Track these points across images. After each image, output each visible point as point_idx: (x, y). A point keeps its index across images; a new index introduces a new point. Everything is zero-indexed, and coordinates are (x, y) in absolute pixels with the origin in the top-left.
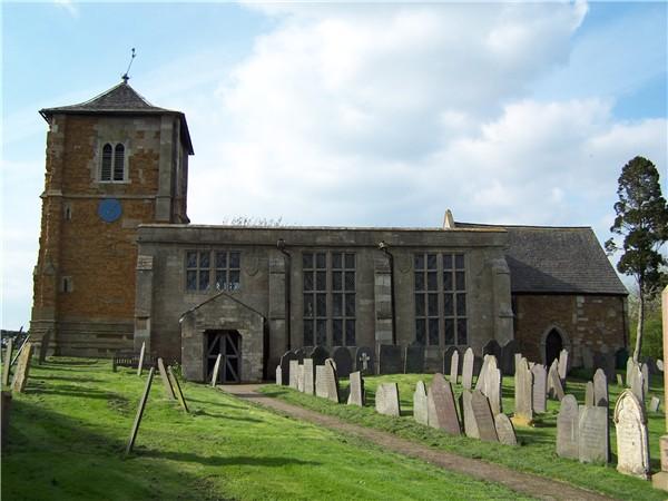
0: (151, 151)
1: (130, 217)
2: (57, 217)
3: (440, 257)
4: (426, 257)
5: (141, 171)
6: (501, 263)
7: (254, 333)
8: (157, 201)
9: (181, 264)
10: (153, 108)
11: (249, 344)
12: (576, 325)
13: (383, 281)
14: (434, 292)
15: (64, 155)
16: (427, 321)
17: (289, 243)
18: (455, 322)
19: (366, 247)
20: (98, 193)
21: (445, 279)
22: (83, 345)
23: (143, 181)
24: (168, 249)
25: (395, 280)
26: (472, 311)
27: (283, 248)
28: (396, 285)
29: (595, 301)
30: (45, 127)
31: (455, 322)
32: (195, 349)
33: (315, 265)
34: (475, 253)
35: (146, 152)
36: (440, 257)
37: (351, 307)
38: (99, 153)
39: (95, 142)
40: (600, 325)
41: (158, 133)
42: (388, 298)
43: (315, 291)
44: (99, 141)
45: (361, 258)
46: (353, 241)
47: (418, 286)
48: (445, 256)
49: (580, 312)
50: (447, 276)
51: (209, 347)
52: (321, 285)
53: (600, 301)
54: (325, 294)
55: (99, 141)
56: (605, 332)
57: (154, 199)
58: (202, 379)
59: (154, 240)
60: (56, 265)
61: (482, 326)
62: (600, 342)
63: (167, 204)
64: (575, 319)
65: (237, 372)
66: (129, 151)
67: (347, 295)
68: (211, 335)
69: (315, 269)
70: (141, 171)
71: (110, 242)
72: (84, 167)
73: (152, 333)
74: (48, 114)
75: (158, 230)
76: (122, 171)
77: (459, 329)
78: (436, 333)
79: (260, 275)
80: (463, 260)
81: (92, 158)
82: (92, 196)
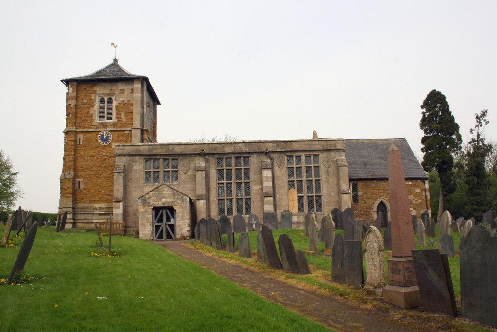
2: (73, 143)
5: (123, 114)
6: (342, 158)
8: (133, 131)
10: (129, 75)
11: (181, 215)
15: (76, 106)
17: (207, 152)
18: (315, 198)
19: (256, 152)
21: (307, 171)
22: (90, 221)
23: (124, 120)
24: (133, 158)
25: (275, 173)
26: (324, 191)
27: (202, 155)
28: (275, 176)
30: (65, 89)
31: (315, 198)
32: (147, 219)
34: (325, 154)
35: (125, 102)
36: (303, 158)
37: (300, 207)
38: (97, 103)
39: (95, 98)
41: (132, 90)
42: (270, 184)
43: (225, 181)
44: (97, 96)
45: (254, 160)
46: (248, 150)
51: (156, 218)
52: (229, 177)
53: (410, 183)
54: (231, 183)
56: (414, 202)
63: (139, 132)
65: (173, 233)
66: (116, 101)
67: (245, 183)
68: (157, 210)
69: (243, 167)
70: (123, 114)
71: (105, 157)
72: (88, 113)
74: (67, 82)
75: (127, 148)
76: (111, 114)
77: (317, 203)
78: (303, 206)
79: (190, 173)
82: (93, 130)
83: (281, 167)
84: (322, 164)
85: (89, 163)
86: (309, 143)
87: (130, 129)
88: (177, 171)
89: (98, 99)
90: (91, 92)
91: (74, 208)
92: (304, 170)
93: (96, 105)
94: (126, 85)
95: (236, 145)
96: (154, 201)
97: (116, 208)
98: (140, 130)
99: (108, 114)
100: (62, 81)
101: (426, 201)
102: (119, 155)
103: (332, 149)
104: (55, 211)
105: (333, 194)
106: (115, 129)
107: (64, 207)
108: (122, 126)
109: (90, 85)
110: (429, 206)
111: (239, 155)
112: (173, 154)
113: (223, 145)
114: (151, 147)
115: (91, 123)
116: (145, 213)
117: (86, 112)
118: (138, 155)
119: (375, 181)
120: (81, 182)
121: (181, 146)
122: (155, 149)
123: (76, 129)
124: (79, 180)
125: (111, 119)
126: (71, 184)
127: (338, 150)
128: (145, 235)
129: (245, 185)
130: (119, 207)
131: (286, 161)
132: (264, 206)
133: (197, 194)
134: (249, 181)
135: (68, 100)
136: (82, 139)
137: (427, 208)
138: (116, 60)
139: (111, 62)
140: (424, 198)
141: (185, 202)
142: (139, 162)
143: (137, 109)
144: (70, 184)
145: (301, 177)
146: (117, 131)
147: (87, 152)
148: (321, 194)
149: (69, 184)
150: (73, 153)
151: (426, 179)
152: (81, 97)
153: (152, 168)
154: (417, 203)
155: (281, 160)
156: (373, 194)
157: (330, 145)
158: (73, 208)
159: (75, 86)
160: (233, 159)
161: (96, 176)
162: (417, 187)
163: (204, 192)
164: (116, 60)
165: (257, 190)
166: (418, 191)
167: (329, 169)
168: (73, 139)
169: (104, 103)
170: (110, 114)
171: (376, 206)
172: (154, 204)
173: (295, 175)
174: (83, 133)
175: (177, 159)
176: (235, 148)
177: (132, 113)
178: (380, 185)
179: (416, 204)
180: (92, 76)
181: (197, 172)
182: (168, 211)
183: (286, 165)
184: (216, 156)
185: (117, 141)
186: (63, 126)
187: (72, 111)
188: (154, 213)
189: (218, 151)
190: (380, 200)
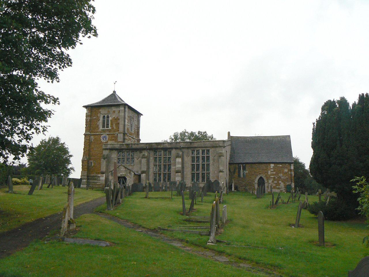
0: (117, 117)
3: (201, 151)
5: (114, 125)
9: (116, 156)
13: (179, 160)
15: (90, 121)
23: (115, 128)
29: (278, 166)
30: (85, 111)
39: (100, 116)
40: (281, 175)
41: (119, 111)
42: (180, 166)
45: (174, 152)
47: (193, 161)
49: (272, 170)
55: (101, 115)
56: (282, 178)
58: (181, 197)
62: (280, 182)
63: (122, 135)
64: (269, 173)
70: (114, 125)
73: (105, 178)
74: (86, 107)
80: (209, 152)
81: (99, 121)
85: (96, 152)
88: (134, 158)
89: (102, 116)
91: (88, 176)
92: (201, 158)
100: (84, 107)
101: (291, 177)
104: (79, 178)
105: (216, 172)
106: (110, 133)
108: (114, 132)
110: (293, 181)
119: (257, 164)
125: (108, 127)
129: (168, 166)
130: (103, 176)
131: (191, 153)
136: (93, 139)
137: (291, 182)
138: (114, 92)
140: (290, 175)
144: (86, 164)
148: (209, 172)
150: (88, 146)
151: (292, 163)
156: (255, 172)
157: (215, 144)
158: (87, 176)
162: (285, 168)
164: (114, 92)
167: (214, 158)
170: (108, 125)
171: (256, 181)
173: (195, 161)
179: (283, 179)
180: (100, 102)
182: (123, 179)
184: (154, 150)
185: (111, 140)
190: (260, 176)
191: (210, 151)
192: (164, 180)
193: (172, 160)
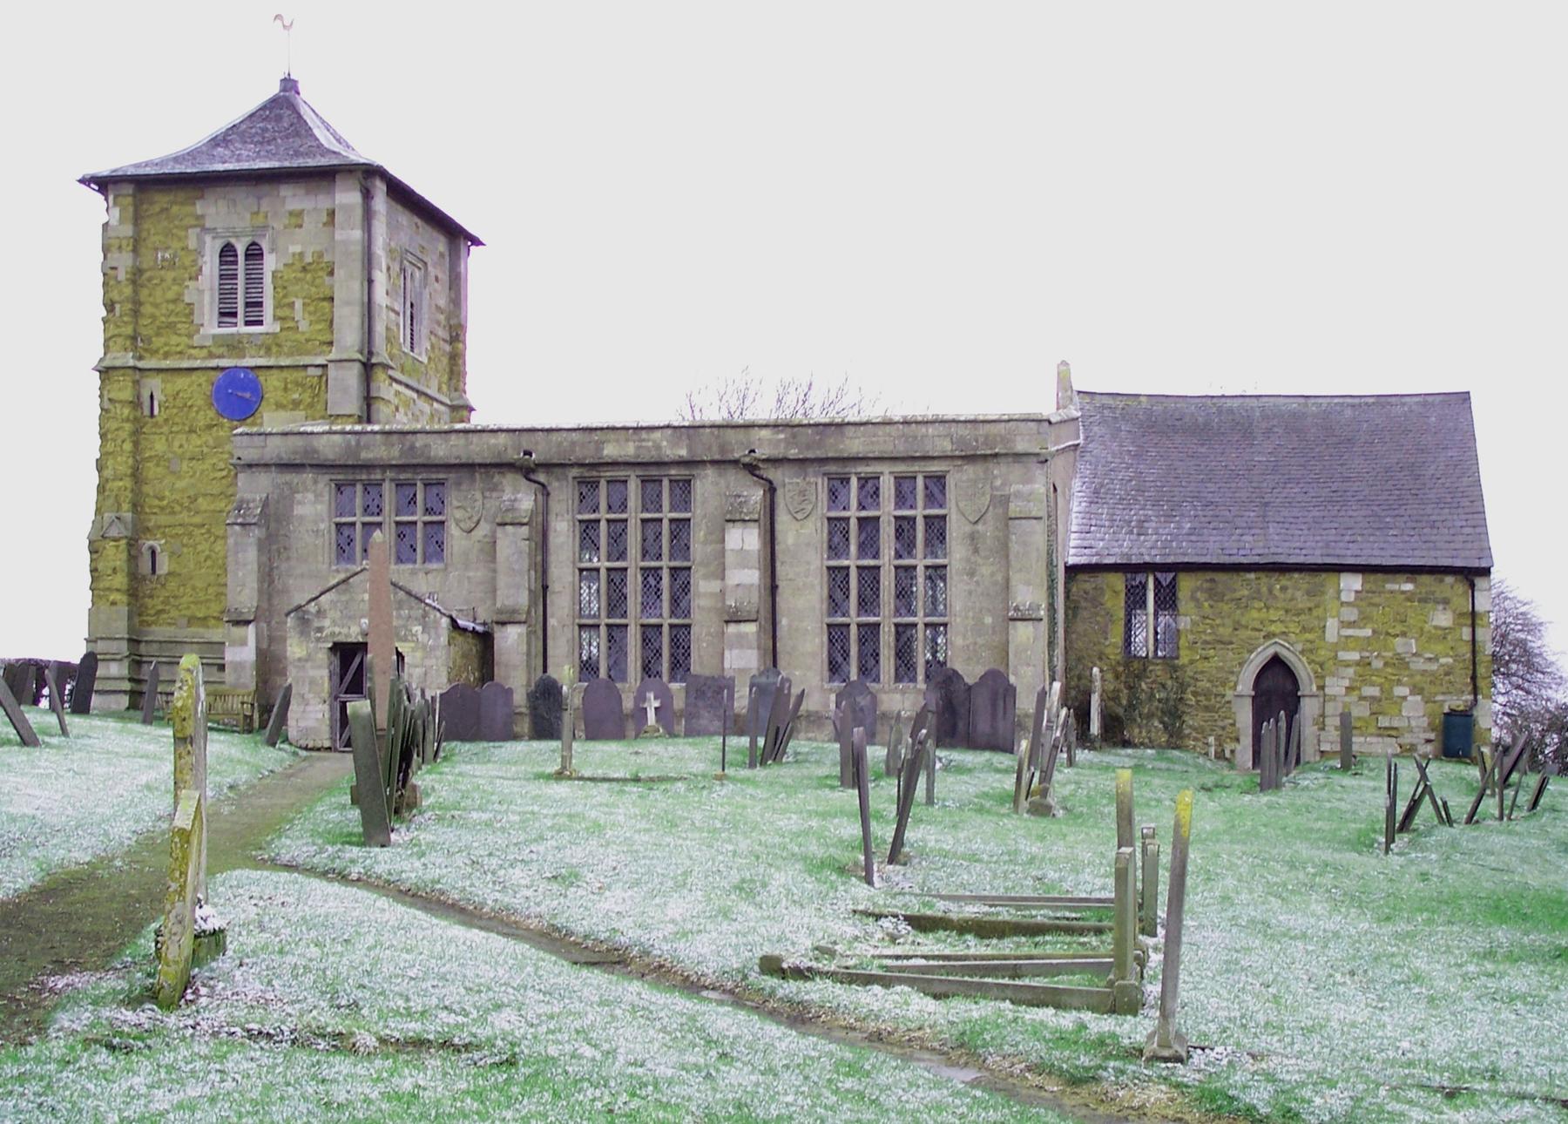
1: (280, 406)
3: (887, 486)
4: (854, 481)
5: (298, 304)
7: (428, 651)
9: (322, 508)
12: (1336, 647)
13: (745, 540)
14: (872, 562)
15: (137, 275)
16: (854, 630)
19: (714, 462)
20: (211, 356)
29: (1389, 586)
30: (95, 208)
32: (312, 682)
33: (603, 506)
34: (971, 471)
35: (309, 259)
36: (887, 486)
38: (210, 265)
39: (201, 242)
41: (332, 214)
44: (208, 238)
45: (708, 488)
47: (836, 547)
48: (899, 480)
49: (1351, 614)
50: (904, 528)
53: (1409, 587)
57: (324, 366)
58: (327, 744)
59: (267, 459)
60: (128, 516)
61: (980, 641)
63: (352, 375)
64: (1332, 633)
67: (673, 570)
69: (603, 514)
70: (298, 304)
73: (260, 653)
74: (103, 183)
76: (260, 304)
79: (483, 530)
82: (197, 364)
83: (799, 516)
84: (954, 510)
86: (906, 429)
87: (320, 360)
89: (212, 249)
90: (187, 221)
91: (134, 642)
92: (887, 532)
93: (206, 270)
94: (308, 193)
95: (644, 435)
96: (334, 623)
97: (233, 644)
98: (357, 367)
99: (248, 305)
102: (250, 466)
103: (996, 455)
106: (271, 362)
107: (102, 639)
108: (298, 350)
109: (181, 195)
111: (654, 472)
112: (424, 466)
113: (596, 437)
114: (352, 439)
115: (190, 336)
116: (307, 660)
117: (170, 295)
118: (312, 466)
119: (1252, 576)
120: (158, 550)
121: (453, 436)
122: (367, 447)
123: (141, 358)
124: (151, 543)
125: (260, 323)
126: (124, 556)
127: (1018, 457)
128: (306, 732)
130: (244, 643)
132: (727, 653)
133: (499, 605)
134: (685, 564)
135: (106, 250)
136: (158, 397)
138: (289, 84)
139: (274, 89)
140: (1466, 651)
141: (432, 632)
142: (314, 491)
143: (347, 287)
145: (876, 556)
146: (281, 367)
147: (176, 444)
149: (116, 556)
150: (128, 446)
152: (155, 239)
153: (359, 511)
154: (1434, 667)
155: (802, 493)
157: (987, 437)
158: (130, 640)
159: (130, 200)
160: (633, 487)
161: (209, 531)
163: (523, 599)
164: (289, 84)
165: (712, 595)
166: (1443, 619)
167: (980, 527)
168: (127, 395)
169: (235, 263)
170: (254, 304)
172: (333, 634)
173: (853, 548)
174: (161, 376)
175: (441, 483)
176: (639, 448)
177: (332, 299)
178: (1270, 591)
181: (499, 530)
183: (823, 508)
184: (575, 472)
186: (94, 351)
187: (120, 293)
188: (337, 662)
189: (579, 454)
190: (1270, 652)
191: (950, 481)
192: (648, 669)
193: (698, 538)
